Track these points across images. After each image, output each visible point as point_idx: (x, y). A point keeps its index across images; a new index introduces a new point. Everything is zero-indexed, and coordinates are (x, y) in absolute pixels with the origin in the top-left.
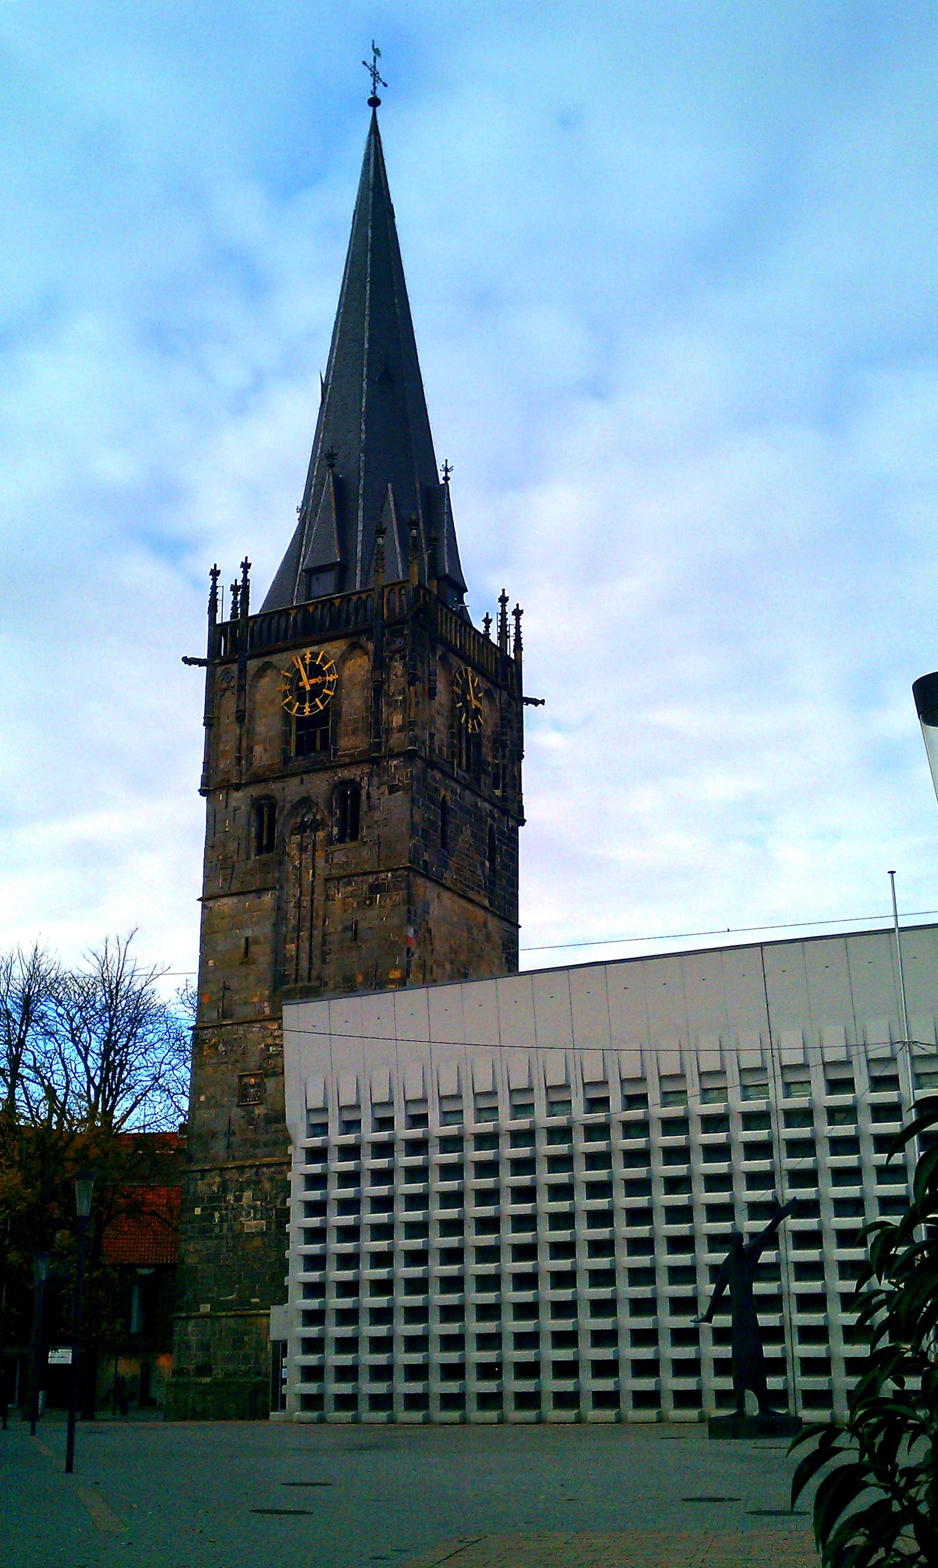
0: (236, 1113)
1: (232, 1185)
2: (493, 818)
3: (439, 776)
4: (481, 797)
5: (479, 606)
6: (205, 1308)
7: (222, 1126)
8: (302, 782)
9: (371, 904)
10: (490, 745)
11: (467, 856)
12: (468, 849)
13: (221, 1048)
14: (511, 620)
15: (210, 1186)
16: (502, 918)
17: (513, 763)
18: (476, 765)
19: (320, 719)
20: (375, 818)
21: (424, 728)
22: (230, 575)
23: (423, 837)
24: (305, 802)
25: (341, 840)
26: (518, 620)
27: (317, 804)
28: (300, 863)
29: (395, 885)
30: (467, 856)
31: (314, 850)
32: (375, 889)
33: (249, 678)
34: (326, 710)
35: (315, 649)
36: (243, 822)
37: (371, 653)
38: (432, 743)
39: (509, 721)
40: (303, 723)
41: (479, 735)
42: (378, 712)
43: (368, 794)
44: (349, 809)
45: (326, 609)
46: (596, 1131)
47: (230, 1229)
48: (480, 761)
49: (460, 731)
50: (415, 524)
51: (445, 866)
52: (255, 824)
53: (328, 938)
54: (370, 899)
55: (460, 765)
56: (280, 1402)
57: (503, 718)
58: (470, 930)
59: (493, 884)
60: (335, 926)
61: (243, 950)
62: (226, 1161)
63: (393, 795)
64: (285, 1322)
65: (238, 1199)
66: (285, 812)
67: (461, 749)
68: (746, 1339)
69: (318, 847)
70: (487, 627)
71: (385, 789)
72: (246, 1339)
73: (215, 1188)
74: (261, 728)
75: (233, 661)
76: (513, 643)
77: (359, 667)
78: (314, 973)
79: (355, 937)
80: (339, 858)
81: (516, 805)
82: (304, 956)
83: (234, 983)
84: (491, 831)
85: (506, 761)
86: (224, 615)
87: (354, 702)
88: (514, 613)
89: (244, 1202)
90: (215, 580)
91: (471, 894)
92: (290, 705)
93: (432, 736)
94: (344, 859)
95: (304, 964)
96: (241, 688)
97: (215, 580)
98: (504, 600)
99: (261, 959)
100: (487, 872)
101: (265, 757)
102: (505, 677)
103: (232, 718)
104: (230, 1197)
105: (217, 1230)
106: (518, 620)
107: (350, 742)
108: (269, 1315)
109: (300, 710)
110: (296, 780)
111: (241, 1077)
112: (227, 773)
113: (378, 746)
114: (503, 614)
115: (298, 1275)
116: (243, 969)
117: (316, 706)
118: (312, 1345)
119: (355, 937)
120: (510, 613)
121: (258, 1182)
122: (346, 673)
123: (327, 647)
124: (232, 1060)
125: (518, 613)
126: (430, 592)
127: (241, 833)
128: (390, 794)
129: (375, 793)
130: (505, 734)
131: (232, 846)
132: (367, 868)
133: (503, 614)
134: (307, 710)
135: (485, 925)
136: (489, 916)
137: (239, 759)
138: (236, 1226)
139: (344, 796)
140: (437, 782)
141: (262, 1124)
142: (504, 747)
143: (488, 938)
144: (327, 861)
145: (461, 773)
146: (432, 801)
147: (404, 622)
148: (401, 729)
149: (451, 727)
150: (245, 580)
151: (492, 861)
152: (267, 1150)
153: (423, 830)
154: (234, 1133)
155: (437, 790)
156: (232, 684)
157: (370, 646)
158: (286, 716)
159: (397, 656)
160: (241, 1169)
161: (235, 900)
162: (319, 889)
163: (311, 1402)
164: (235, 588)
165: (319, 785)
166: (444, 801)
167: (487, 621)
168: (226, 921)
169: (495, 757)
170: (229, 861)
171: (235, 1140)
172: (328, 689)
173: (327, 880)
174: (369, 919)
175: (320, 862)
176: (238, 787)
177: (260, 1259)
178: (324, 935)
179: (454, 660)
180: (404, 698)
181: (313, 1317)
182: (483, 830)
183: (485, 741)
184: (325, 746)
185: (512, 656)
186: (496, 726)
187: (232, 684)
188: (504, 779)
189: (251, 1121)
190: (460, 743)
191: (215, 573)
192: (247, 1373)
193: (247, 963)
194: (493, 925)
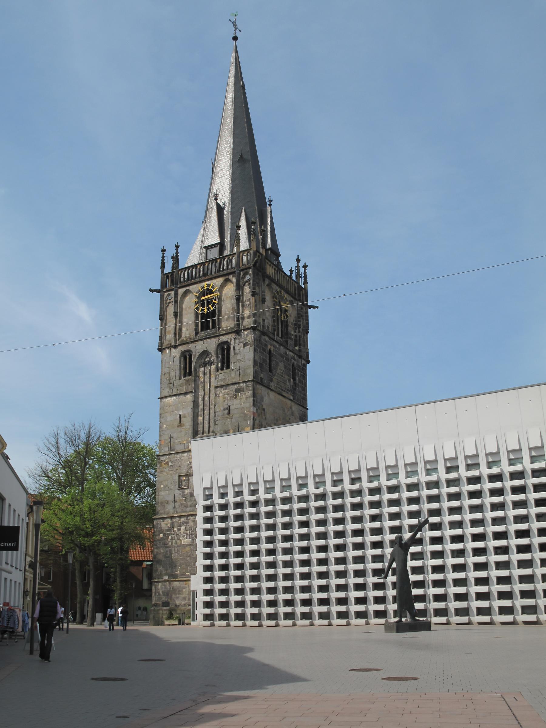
0: (178, 492)
1: (176, 524)
2: (294, 359)
3: (267, 339)
4: (288, 349)
5: (287, 264)
6: (166, 577)
7: (171, 498)
8: (204, 343)
9: (236, 397)
10: (293, 326)
11: (282, 376)
12: (282, 373)
13: (170, 464)
14: (302, 270)
15: (167, 524)
16: (300, 405)
17: (304, 335)
18: (286, 334)
19: (212, 314)
20: (238, 359)
21: (260, 317)
22: (170, 252)
23: (260, 367)
24: (205, 353)
25: (222, 369)
26: (305, 270)
27: (211, 353)
28: (204, 380)
29: (247, 389)
30: (282, 376)
31: (210, 374)
32: (238, 391)
33: (179, 297)
34: (214, 310)
35: (208, 282)
36: (178, 362)
37: (235, 283)
38: (264, 324)
39: (302, 316)
40: (203, 316)
41: (287, 322)
42: (238, 309)
43: (234, 348)
44: (225, 354)
45: (214, 263)
46: (337, 495)
47: (176, 543)
48: (287, 333)
49: (278, 319)
50: (254, 223)
51: (271, 380)
52: (182, 363)
53: (217, 413)
54: (236, 395)
55: (278, 335)
56: (195, 618)
57: (298, 314)
58: (284, 410)
59: (295, 389)
60: (220, 408)
61: (179, 421)
62: (173, 514)
63: (246, 347)
64: (197, 583)
65: (179, 530)
66: (197, 357)
67: (278, 328)
68: (403, 585)
69: (212, 373)
70: (291, 274)
71: (241, 345)
72: (184, 590)
73: (169, 525)
74: (185, 320)
75: (172, 290)
76: (303, 281)
77: (230, 290)
78: (211, 430)
79: (229, 413)
80: (221, 377)
81: (305, 354)
82: (206, 422)
83: (175, 435)
84: (293, 365)
85: (300, 334)
86: (168, 269)
87: (228, 306)
88: (303, 267)
89: (182, 531)
90: (163, 254)
91: (284, 394)
92: (197, 308)
93: (264, 320)
94: (223, 377)
95: (206, 426)
96: (176, 302)
97: (163, 254)
98: (298, 260)
99: (187, 424)
100: (292, 384)
101: (187, 332)
102: (299, 295)
103: (172, 316)
104: (176, 529)
105: (170, 543)
106: (305, 270)
107: (227, 324)
108: (190, 580)
109: (202, 310)
110: (201, 342)
111: (179, 476)
112: (170, 341)
113: (238, 325)
114: (298, 267)
115: (201, 562)
116: (179, 429)
117: (210, 308)
118: (208, 592)
119: (229, 413)
120: (302, 267)
121: (187, 523)
122: (224, 293)
123: (215, 281)
124: (175, 469)
125: (305, 267)
126: (262, 255)
127: (177, 367)
128: (244, 347)
129: (236, 345)
130: (299, 321)
131: (173, 374)
132: (234, 381)
133: (298, 267)
134: (206, 310)
135: (291, 408)
136: (293, 404)
137: (175, 334)
138: (178, 542)
139: (223, 349)
140: (266, 342)
141: (189, 497)
142: (299, 327)
143: (293, 414)
144: (216, 379)
145: (278, 338)
146: (265, 350)
147: (250, 268)
148: (249, 317)
149: (273, 317)
150: (177, 253)
151: (294, 379)
152: (191, 508)
153: (260, 363)
154: (176, 501)
155: (266, 345)
156: (172, 300)
157: (234, 280)
158: (197, 314)
159: (247, 284)
160: (180, 517)
161: (175, 398)
162: (213, 392)
163: (208, 617)
164: (173, 258)
165: (211, 345)
166: (270, 351)
167: (291, 271)
168: (171, 407)
169: (295, 332)
170: (171, 381)
171: (177, 504)
172: (215, 300)
173: (216, 387)
174: (235, 405)
175: (213, 379)
176: (175, 347)
177: (189, 556)
178: (215, 412)
179: (275, 286)
180: (250, 303)
181: (209, 580)
182: (289, 365)
183: (290, 324)
184: (214, 327)
185: (303, 286)
186: (296, 318)
187: (172, 300)
188: (300, 341)
189: (184, 496)
190: (278, 325)
191: (163, 251)
192: (185, 605)
193: (181, 426)
194: (295, 408)
